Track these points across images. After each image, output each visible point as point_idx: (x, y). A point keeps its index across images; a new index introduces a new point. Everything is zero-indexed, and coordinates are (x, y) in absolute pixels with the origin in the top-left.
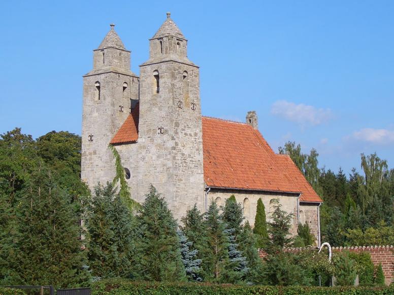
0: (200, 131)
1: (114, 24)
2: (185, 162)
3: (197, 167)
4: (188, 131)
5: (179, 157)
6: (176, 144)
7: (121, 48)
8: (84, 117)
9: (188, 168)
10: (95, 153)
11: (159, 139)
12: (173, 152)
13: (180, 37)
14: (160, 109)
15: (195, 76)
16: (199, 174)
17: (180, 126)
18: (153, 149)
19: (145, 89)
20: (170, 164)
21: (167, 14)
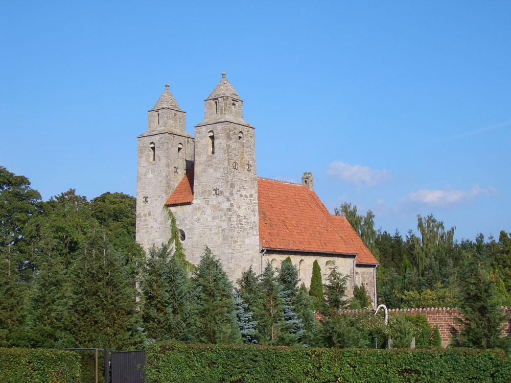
0: (256, 193)
1: (169, 85)
2: (241, 224)
3: (252, 228)
4: (244, 193)
5: (234, 218)
6: (232, 205)
7: (176, 109)
8: (139, 179)
10: (150, 214)
11: (214, 200)
12: (228, 213)
13: (235, 97)
15: (250, 137)
16: (255, 235)
18: (209, 211)
19: (200, 149)
21: (222, 74)
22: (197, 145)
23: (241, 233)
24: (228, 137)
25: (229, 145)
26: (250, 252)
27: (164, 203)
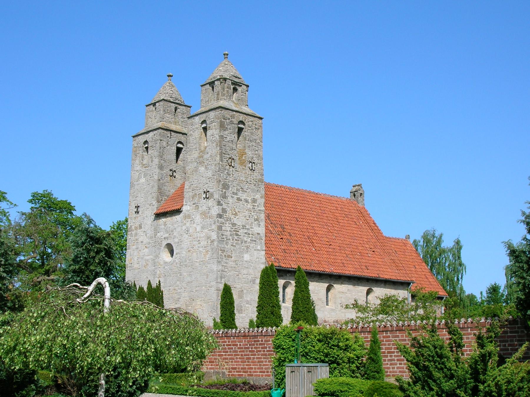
0: (261, 197)
1: (171, 74)
2: (237, 235)
3: (255, 241)
4: (243, 196)
5: (227, 227)
6: (224, 210)
7: (177, 101)
8: (132, 185)
9: (242, 243)
10: (140, 227)
11: (204, 205)
12: (218, 221)
13: (237, 80)
14: (206, 168)
15: (256, 128)
16: (258, 250)
17: (230, 189)
18: (198, 218)
19: (192, 145)
20: (214, 236)
21: (224, 54)
22: (190, 139)
23: (237, 246)
24: (222, 126)
25: (222, 136)
26: (251, 271)
27: (155, 211)
